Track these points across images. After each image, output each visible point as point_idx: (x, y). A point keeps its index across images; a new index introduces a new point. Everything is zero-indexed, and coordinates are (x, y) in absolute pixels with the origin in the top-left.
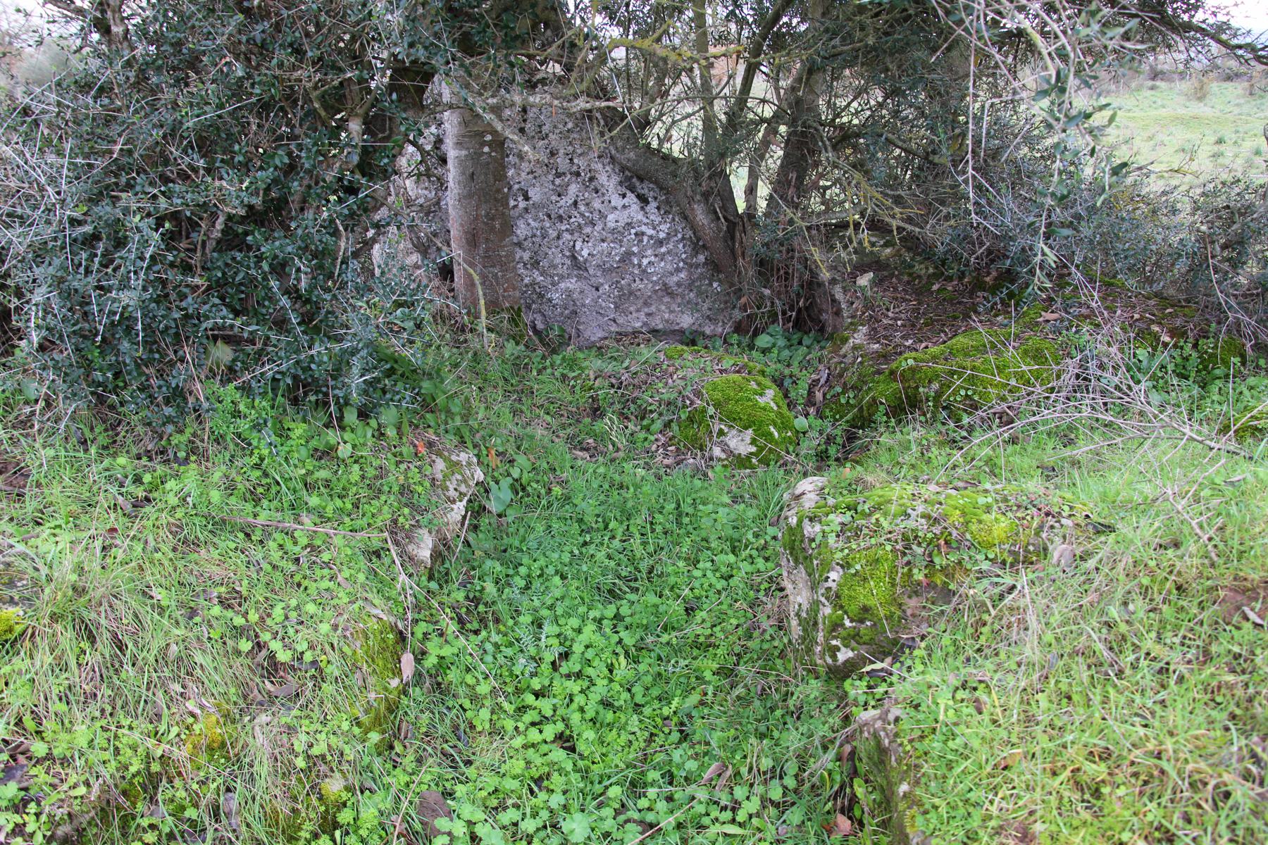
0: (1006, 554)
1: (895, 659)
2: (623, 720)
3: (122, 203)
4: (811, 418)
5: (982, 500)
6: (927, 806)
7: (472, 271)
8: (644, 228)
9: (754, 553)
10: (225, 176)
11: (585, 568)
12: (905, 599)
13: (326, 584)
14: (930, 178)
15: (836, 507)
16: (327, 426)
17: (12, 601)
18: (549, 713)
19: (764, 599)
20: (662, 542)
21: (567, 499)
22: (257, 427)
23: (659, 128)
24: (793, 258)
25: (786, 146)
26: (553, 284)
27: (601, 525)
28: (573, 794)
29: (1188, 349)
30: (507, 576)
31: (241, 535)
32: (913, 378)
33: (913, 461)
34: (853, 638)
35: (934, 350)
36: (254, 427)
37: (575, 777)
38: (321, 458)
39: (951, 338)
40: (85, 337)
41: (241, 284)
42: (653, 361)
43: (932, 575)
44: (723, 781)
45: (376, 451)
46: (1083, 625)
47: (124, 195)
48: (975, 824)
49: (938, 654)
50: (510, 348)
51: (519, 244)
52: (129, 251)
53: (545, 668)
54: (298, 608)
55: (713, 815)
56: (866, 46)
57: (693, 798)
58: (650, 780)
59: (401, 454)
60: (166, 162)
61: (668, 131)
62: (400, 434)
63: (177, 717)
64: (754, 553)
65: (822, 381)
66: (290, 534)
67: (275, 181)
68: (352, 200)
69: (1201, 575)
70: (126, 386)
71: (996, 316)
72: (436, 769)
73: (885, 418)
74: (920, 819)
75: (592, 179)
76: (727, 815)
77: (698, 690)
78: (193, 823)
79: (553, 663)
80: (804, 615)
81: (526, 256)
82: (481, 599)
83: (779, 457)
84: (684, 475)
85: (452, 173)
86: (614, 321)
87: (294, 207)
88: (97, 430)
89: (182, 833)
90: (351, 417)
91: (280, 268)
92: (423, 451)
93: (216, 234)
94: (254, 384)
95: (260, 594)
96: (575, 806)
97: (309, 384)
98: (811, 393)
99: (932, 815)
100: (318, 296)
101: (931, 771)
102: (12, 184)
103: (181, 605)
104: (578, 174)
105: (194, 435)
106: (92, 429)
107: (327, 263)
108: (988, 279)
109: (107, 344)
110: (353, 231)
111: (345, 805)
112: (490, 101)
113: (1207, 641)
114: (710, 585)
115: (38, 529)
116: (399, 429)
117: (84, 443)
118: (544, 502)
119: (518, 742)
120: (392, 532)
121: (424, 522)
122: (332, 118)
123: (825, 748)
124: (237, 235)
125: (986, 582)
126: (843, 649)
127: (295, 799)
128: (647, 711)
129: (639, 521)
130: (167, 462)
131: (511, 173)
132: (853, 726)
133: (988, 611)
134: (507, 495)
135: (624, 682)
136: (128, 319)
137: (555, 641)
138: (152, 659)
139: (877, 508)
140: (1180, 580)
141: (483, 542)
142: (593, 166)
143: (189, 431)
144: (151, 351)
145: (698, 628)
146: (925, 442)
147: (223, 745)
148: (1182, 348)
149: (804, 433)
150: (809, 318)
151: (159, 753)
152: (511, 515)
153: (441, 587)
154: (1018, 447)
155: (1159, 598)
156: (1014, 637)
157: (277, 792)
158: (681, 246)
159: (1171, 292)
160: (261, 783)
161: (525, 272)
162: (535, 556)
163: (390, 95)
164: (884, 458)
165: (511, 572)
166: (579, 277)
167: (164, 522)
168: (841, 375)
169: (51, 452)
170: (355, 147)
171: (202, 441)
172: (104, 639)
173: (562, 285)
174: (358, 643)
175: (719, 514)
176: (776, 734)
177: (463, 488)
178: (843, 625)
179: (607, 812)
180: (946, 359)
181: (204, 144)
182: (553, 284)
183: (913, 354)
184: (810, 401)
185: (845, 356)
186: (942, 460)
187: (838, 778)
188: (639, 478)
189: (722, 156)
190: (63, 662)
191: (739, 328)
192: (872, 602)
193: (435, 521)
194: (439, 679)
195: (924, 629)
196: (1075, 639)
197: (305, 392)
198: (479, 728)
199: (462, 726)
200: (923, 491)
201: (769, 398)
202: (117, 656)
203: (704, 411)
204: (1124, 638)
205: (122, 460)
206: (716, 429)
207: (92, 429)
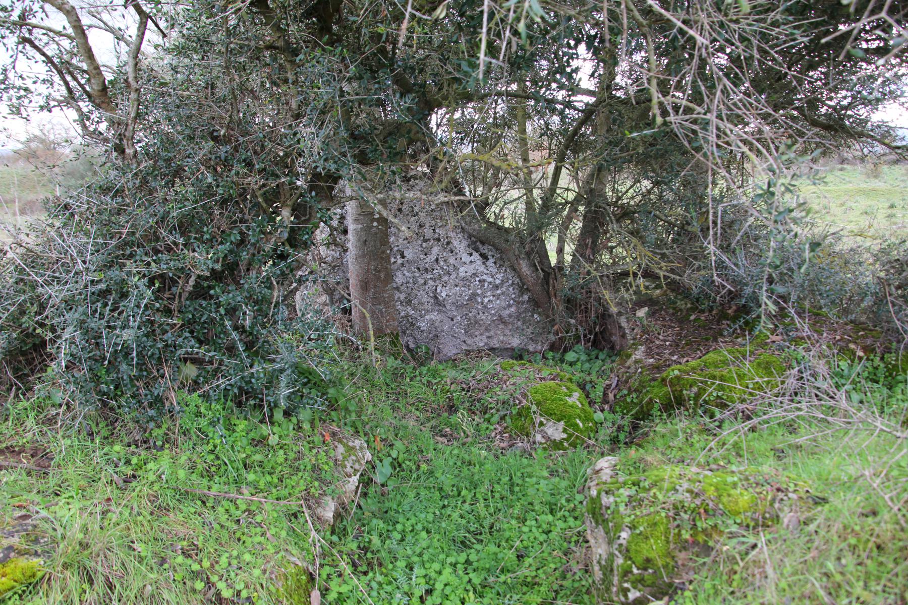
0: (749, 520)
3: (127, 269)
4: (606, 412)
5: (730, 479)
7: (364, 311)
8: (485, 277)
9: (567, 514)
10: (197, 249)
12: (677, 553)
13: (258, 539)
14: (686, 241)
15: (625, 483)
16: (261, 422)
17: (36, 554)
19: (574, 549)
21: (431, 473)
22: (213, 424)
23: (495, 209)
24: (590, 297)
25: (584, 220)
27: (455, 493)
29: (877, 361)
30: (388, 531)
31: (199, 503)
33: (681, 445)
35: (693, 363)
36: (211, 423)
38: (256, 445)
39: (704, 355)
40: (96, 360)
41: (205, 322)
42: (493, 372)
43: (696, 533)
46: (807, 575)
47: (128, 262)
49: (702, 596)
50: (391, 362)
51: (397, 289)
52: (130, 301)
54: (238, 557)
56: (638, 153)
59: (313, 442)
60: (157, 239)
61: (501, 210)
62: (313, 427)
64: (567, 514)
65: (613, 386)
66: (233, 501)
67: (231, 252)
68: (282, 264)
69: (894, 538)
70: (124, 395)
71: (737, 338)
73: (659, 413)
75: (448, 243)
79: (421, 597)
80: (603, 563)
81: (402, 296)
82: (369, 548)
83: (583, 441)
84: (515, 455)
85: (351, 240)
86: (464, 342)
87: (243, 267)
88: (101, 426)
90: (278, 415)
91: (232, 311)
92: (329, 439)
93: (189, 288)
95: (211, 547)
97: (250, 392)
98: (605, 394)
100: (258, 331)
102: (54, 256)
103: (155, 554)
104: (439, 240)
105: (169, 429)
106: (97, 425)
107: (264, 307)
108: (729, 312)
109: (113, 365)
110: (282, 284)
112: (379, 196)
113: (903, 589)
114: (535, 538)
115: (57, 498)
116: (312, 423)
117: (91, 434)
118: (415, 475)
120: (306, 500)
121: (329, 491)
122: (271, 206)
124: (203, 288)
125: (735, 540)
126: (632, 590)
129: (483, 490)
130: (148, 448)
131: (392, 239)
133: (737, 563)
134: (388, 470)
136: (127, 348)
137: (423, 581)
138: (133, 596)
139: (654, 485)
140: (879, 541)
141: (370, 505)
142: (451, 234)
143: (165, 426)
144: (141, 370)
145: (525, 571)
146: (688, 431)
148: (872, 360)
149: (601, 424)
150: (602, 339)
153: (340, 539)
154: (756, 434)
155: (864, 555)
156: (757, 583)
158: (511, 289)
159: (863, 319)
161: (402, 308)
162: (408, 516)
163: (310, 193)
164: (659, 443)
165: (391, 528)
166: (440, 311)
168: (626, 382)
169: (68, 442)
170: (286, 227)
171: (174, 433)
172: (100, 581)
173: (428, 317)
174: (280, 583)
175: (540, 485)
177: (357, 466)
178: (631, 572)
180: (702, 370)
181: (184, 227)
182: (421, 316)
183: (678, 366)
184: (605, 400)
185: (629, 368)
186: (702, 444)
188: (483, 457)
190: (69, 600)
191: (553, 347)
192: (652, 555)
195: (692, 576)
196: (803, 586)
197: (247, 398)
200: (687, 472)
201: (575, 398)
202: (108, 594)
203: (529, 408)
204: (839, 586)
205: (117, 448)
206: (537, 422)
207: (97, 425)
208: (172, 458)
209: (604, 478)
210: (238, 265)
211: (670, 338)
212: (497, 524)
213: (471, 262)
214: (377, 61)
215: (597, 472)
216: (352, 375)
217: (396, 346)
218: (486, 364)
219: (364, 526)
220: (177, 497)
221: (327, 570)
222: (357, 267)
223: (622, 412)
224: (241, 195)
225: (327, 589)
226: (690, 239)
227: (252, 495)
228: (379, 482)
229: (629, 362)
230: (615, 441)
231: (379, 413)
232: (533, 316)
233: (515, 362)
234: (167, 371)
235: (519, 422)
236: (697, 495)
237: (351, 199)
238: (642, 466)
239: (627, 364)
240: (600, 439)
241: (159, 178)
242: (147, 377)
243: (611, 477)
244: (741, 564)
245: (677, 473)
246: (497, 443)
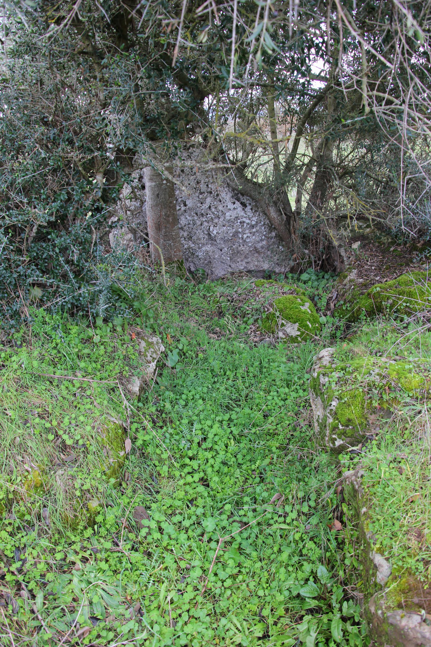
1: (363, 445)
2: (232, 471)
6: (374, 519)
8: (244, 219)
11: (214, 395)
13: (89, 406)
15: (336, 369)
16: (88, 326)
18: (196, 468)
19: (302, 411)
20: (253, 382)
22: (54, 329)
26: (199, 248)
27: (222, 372)
28: (208, 508)
31: (48, 383)
32: (379, 297)
34: (343, 434)
35: (391, 282)
36: (53, 329)
37: (209, 500)
39: (399, 276)
41: (45, 258)
42: (249, 288)
43: (381, 403)
44: (280, 502)
45: (112, 338)
48: (396, 529)
50: (178, 281)
51: (182, 228)
53: (195, 445)
54: (75, 418)
55: (275, 519)
57: (266, 511)
58: (245, 501)
59: (124, 340)
60: (8, 199)
62: (123, 330)
63: (20, 472)
64: (298, 387)
65: (334, 298)
67: (61, 207)
68: (98, 215)
71: (422, 264)
72: (142, 496)
73: (365, 318)
74: (371, 526)
75: (218, 195)
76: (282, 519)
77: (269, 456)
78: (29, 522)
79: (199, 443)
80: (320, 421)
81: (185, 234)
83: (311, 338)
87: (70, 217)
89: (24, 527)
90: (99, 322)
91: (64, 250)
92: (135, 337)
93: (33, 234)
94: (52, 307)
95: (57, 411)
96: (209, 514)
98: (328, 304)
99: (377, 523)
101: (377, 502)
104: (211, 193)
105: (25, 333)
107: (87, 246)
108: (418, 245)
110: (99, 229)
111: (99, 513)
112: (165, 164)
116: (123, 326)
118: (195, 361)
119: (182, 482)
121: (135, 373)
123: (329, 487)
124: (43, 233)
125: (408, 408)
126: (338, 440)
127: (75, 510)
128: (244, 467)
129: (241, 371)
131: (177, 192)
132: (342, 477)
134: (176, 358)
135: (233, 452)
137: (200, 432)
138: (8, 445)
141: (164, 382)
142: (219, 189)
143: (22, 331)
145: (267, 427)
146: (384, 330)
147: (42, 485)
150: (328, 265)
151: (12, 489)
152: (179, 367)
153: (144, 405)
157: (67, 507)
158: (263, 228)
160: (60, 503)
162: (190, 389)
165: (178, 397)
166: (212, 244)
167: (12, 377)
168: (343, 295)
170: (100, 188)
171: (28, 336)
173: (204, 249)
174: (104, 435)
175: (280, 368)
176: (306, 479)
177: (154, 356)
179: (224, 517)
180: (396, 287)
181: (26, 190)
183: (380, 285)
184: (328, 308)
185: (345, 285)
186: (393, 340)
187: (335, 502)
188: (241, 348)
189: (283, 185)
191: (292, 270)
192: (352, 417)
193: (141, 373)
194: (144, 451)
195: (378, 431)
197: (77, 311)
198: (163, 475)
199: (155, 474)
200: (379, 361)
201: (307, 307)
208: (28, 353)
209: (325, 363)
210: (67, 216)
211: (375, 264)
212: (251, 394)
213: (234, 209)
214: (161, 66)
215: (320, 359)
216: (151, 291)
217: (181, 270)
218: (245, 282)
219: (160, 396)
220: (33, 379)
221: (135, 426)
222: (153, 214)
223: (339, 316)
224: (66, 165)
225: (136, 438)
226: (393, 191)
227: (84, 377)
228: (170, 366)
229: (346, 281)
230: (333, 336)
231: (169, 318)
232: (278, 247)
233: (265, 281)
234: (21, 293)
235: (267, 324)
236: (384, 377)
237: (146, 166)
238: (351, 355)
239: (344, 283)
240: (324, 335)
241: (7, 154)
242: (7, 298)
243: (329, 362)
244: (411, 424)
245: (372, 362)
246: (252, 338)
